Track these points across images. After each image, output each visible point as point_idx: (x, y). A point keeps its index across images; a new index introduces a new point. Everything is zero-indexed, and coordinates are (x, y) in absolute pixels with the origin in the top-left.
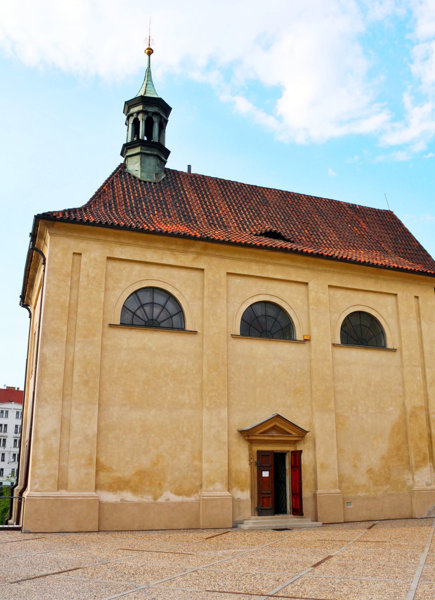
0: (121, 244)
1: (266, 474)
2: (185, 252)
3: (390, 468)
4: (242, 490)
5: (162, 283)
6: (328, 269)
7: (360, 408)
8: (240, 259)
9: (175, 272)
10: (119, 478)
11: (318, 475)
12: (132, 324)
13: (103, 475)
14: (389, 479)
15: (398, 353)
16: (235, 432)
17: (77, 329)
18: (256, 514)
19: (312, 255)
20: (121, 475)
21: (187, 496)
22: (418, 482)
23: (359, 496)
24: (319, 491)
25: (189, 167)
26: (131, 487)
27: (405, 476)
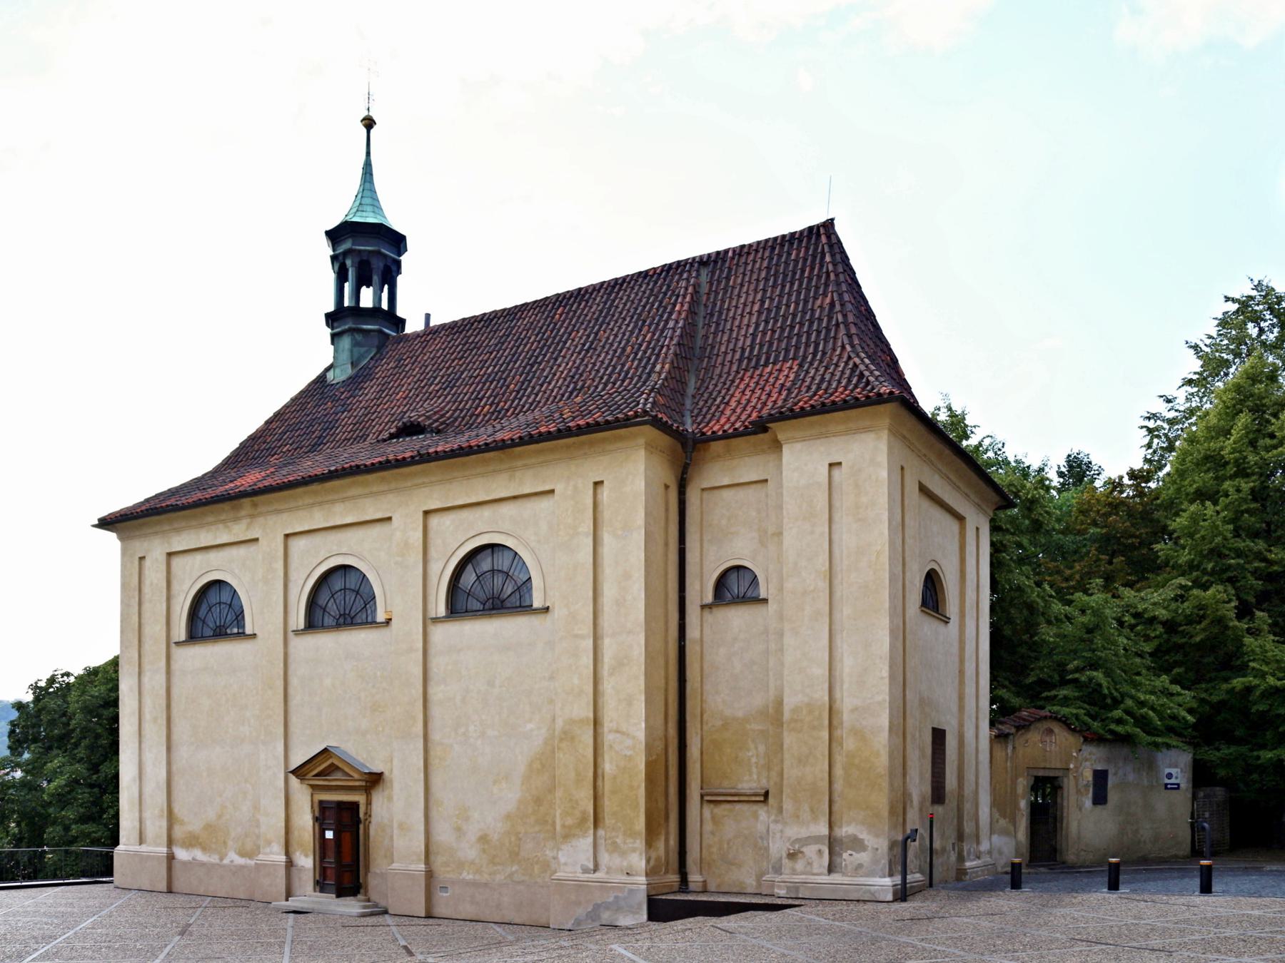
1: (329, 835)
2: (236, 520)
3: (521, 836)
4: (306, 856)
6: (420, 481)
7: (472, 728)
8: (298, 508)
9: (234, 551)
10: (190, 832)
14: (517, 854)
18: (318, 889)
19: (413, 461)
20: (191, 829)
21: (250, 859)
22: (565, 864)
23: (464, 879)
25: (428, 317)
27: (547, 852)
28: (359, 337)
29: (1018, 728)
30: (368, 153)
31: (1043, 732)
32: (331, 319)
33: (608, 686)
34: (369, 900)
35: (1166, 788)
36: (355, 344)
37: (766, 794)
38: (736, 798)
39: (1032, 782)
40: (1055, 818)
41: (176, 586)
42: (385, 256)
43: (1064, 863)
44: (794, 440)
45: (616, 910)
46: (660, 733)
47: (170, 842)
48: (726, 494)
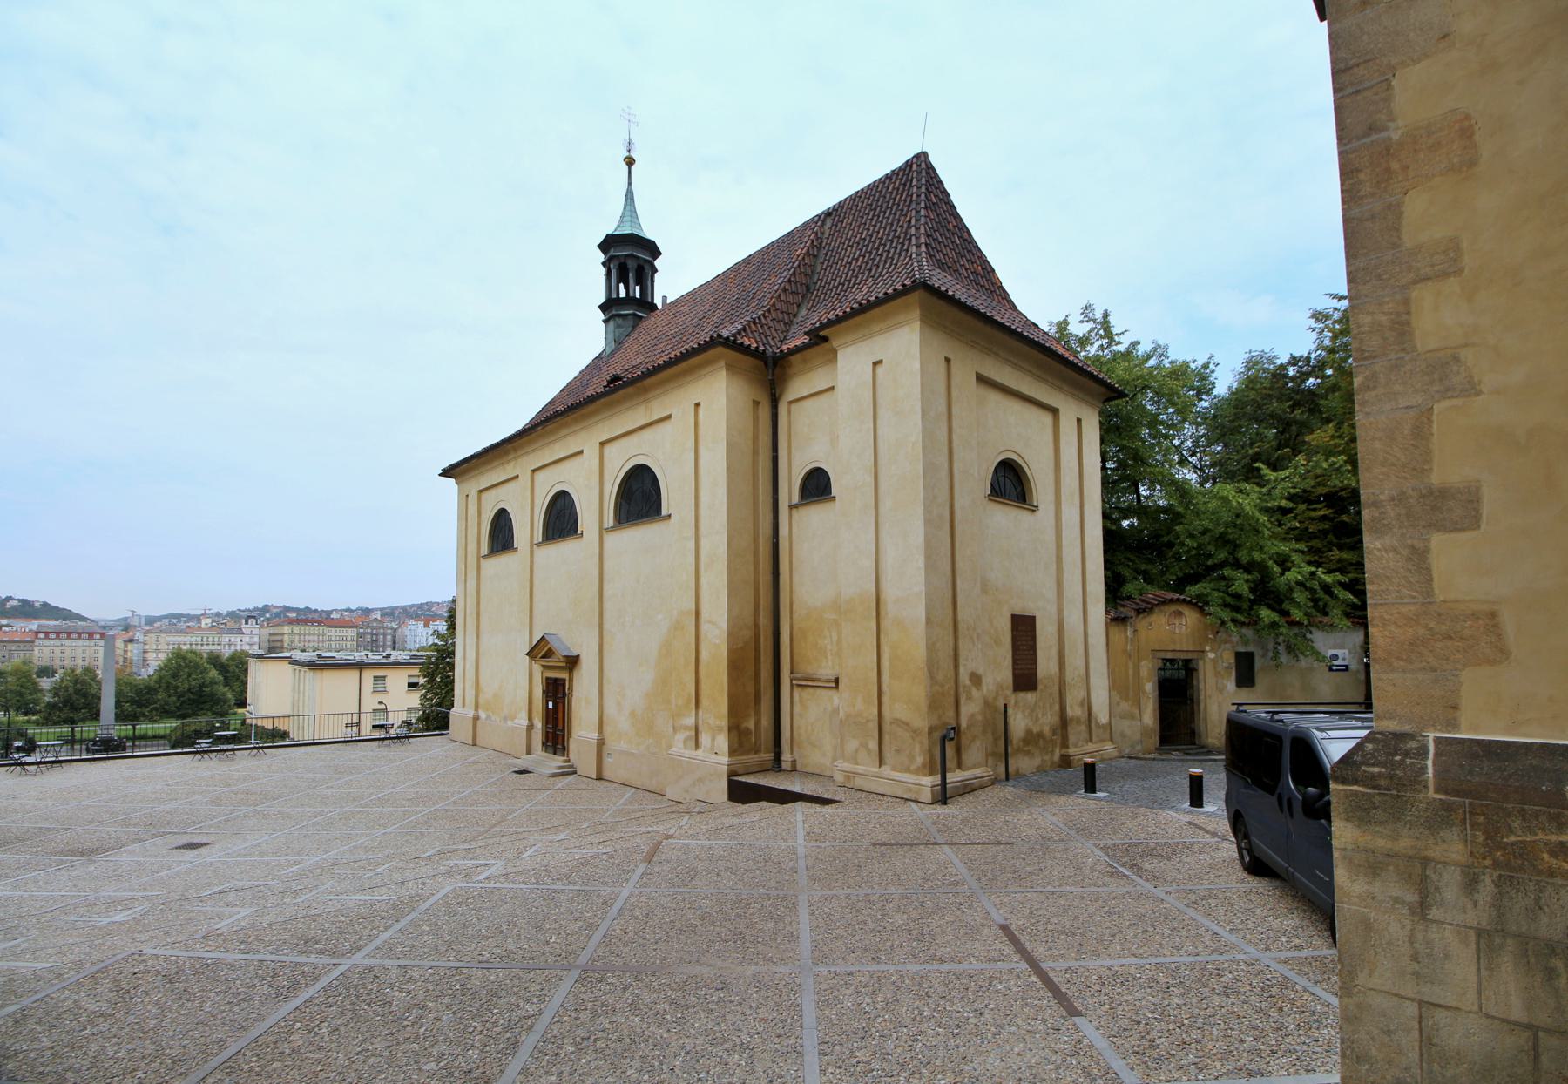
1: (550, 705)
8: (533, 451)
28: (619, 321)
29: (1139, 612)
30: (630, 184)
31: (1170, 615)
32: (603, 308)
33: (704, 581)
34: (569, 761)
35: (1331, 670)
36: (618, 326)
37: (837, 681)
38: (815, 684)
39: (1160, 664)
40: (1192, 700)
41: (483, 516)
42: (638, 258)
43: (1203, 747)
44: (847, 345)
45: (1054, 730)
46: (750, 620)
47: (477, 707)
48: (807, 403)
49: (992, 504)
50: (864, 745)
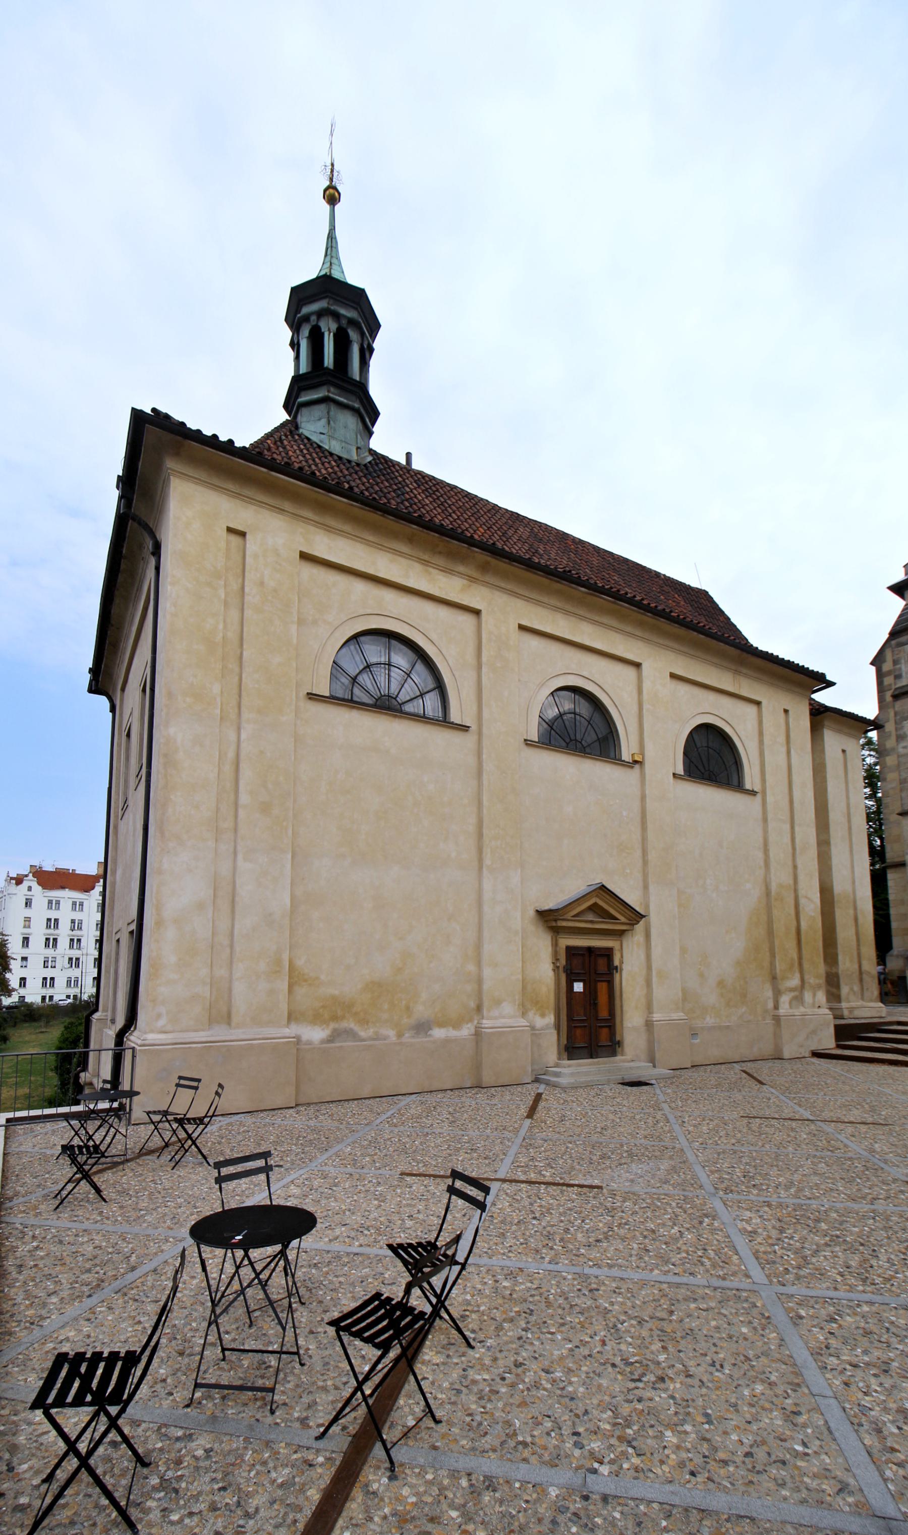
0: (328, 529)
1: (578, 987)
4: (543, 1015)
5: (407, 627)
8: (538, 603)
11: (655, 990)
12: (352, 701)
13: (301, 991)
15: (759, 796)
16: (532, 913)
17: (244, 693)
20: (337, 992)
24: (656, 1016)
26: (356, 1014)
49: (309, 701)
50: (852, 989)
